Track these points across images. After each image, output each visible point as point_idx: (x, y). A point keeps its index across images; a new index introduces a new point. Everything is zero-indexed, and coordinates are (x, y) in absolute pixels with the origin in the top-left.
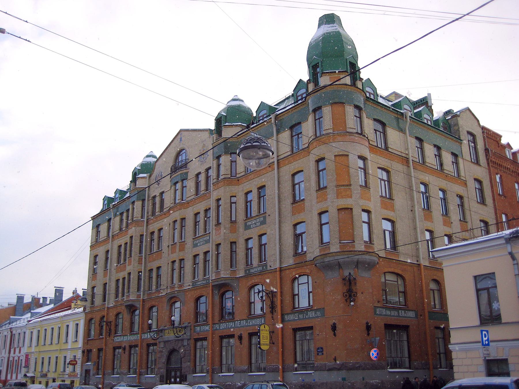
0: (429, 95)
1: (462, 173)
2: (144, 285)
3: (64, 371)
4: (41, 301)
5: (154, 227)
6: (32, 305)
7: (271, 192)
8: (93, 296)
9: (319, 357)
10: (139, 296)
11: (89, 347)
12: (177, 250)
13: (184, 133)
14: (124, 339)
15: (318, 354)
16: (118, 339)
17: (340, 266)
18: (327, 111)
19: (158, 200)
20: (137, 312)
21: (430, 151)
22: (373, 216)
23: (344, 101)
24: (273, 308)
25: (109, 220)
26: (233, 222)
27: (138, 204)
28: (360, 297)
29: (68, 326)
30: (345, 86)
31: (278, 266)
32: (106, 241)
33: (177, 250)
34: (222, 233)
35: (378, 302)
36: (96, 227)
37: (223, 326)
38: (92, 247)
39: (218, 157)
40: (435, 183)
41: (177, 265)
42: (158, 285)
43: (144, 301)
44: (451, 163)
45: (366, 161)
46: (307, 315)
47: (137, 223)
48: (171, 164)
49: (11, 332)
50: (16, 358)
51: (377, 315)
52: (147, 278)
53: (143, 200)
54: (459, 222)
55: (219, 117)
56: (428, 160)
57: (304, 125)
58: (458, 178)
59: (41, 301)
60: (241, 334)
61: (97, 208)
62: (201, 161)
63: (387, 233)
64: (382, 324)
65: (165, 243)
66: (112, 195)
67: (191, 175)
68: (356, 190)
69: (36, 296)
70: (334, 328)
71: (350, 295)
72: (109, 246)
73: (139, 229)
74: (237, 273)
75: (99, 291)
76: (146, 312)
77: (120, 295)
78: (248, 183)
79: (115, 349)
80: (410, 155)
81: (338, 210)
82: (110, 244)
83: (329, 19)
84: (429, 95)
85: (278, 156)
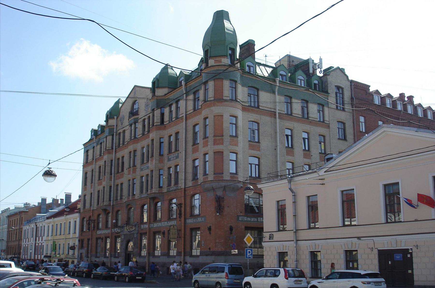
1: (327, 118)
3: (68, 254)
4: (59, 202)
7: (182, 136)
8: (85, 201)
11: (82, 238)
12: (131, 172)
13: (137, 88)
16: (99, 232)
17: (214, 189)
19: (122, 135)
20: (110, 215)
22: (239, 156)
24: (180, 214)
25: (94, 147)
26: (161, 155)
28: (226, 210)
29: (70, 222)
32: (91, 163)
33: (131, 172)
34: (154, 164)
35: (241, 212)
36: (86, 152)
37: (155, 225)
38: (84, 166)
39: (153, 110)
41: (131, 182)
42: (121, 196)
44: (316, 111)
47: (109, 151)
48: (129, 110)
49: (36, 226)
50: (40, 244)
52: (115, 190)
53: (113, 135)
54: (318, 155)
56: (294, 112)
57: (200, 91)
58: (322, 123)
59: (59, 202)
60: (164, 231)
61: (88, 137)
64: (243, 227)
65: (126, 166)
66: (96, 128)
68: (227, 139)
70: (210, 229)
71: (220, 208)
72: (93, 166)
75: (88, 198)
76: (114, 214)
77: (144, 191)
79: (97, 239)
80: (278, 108)
81: (214, 153)
85: (186, 112)
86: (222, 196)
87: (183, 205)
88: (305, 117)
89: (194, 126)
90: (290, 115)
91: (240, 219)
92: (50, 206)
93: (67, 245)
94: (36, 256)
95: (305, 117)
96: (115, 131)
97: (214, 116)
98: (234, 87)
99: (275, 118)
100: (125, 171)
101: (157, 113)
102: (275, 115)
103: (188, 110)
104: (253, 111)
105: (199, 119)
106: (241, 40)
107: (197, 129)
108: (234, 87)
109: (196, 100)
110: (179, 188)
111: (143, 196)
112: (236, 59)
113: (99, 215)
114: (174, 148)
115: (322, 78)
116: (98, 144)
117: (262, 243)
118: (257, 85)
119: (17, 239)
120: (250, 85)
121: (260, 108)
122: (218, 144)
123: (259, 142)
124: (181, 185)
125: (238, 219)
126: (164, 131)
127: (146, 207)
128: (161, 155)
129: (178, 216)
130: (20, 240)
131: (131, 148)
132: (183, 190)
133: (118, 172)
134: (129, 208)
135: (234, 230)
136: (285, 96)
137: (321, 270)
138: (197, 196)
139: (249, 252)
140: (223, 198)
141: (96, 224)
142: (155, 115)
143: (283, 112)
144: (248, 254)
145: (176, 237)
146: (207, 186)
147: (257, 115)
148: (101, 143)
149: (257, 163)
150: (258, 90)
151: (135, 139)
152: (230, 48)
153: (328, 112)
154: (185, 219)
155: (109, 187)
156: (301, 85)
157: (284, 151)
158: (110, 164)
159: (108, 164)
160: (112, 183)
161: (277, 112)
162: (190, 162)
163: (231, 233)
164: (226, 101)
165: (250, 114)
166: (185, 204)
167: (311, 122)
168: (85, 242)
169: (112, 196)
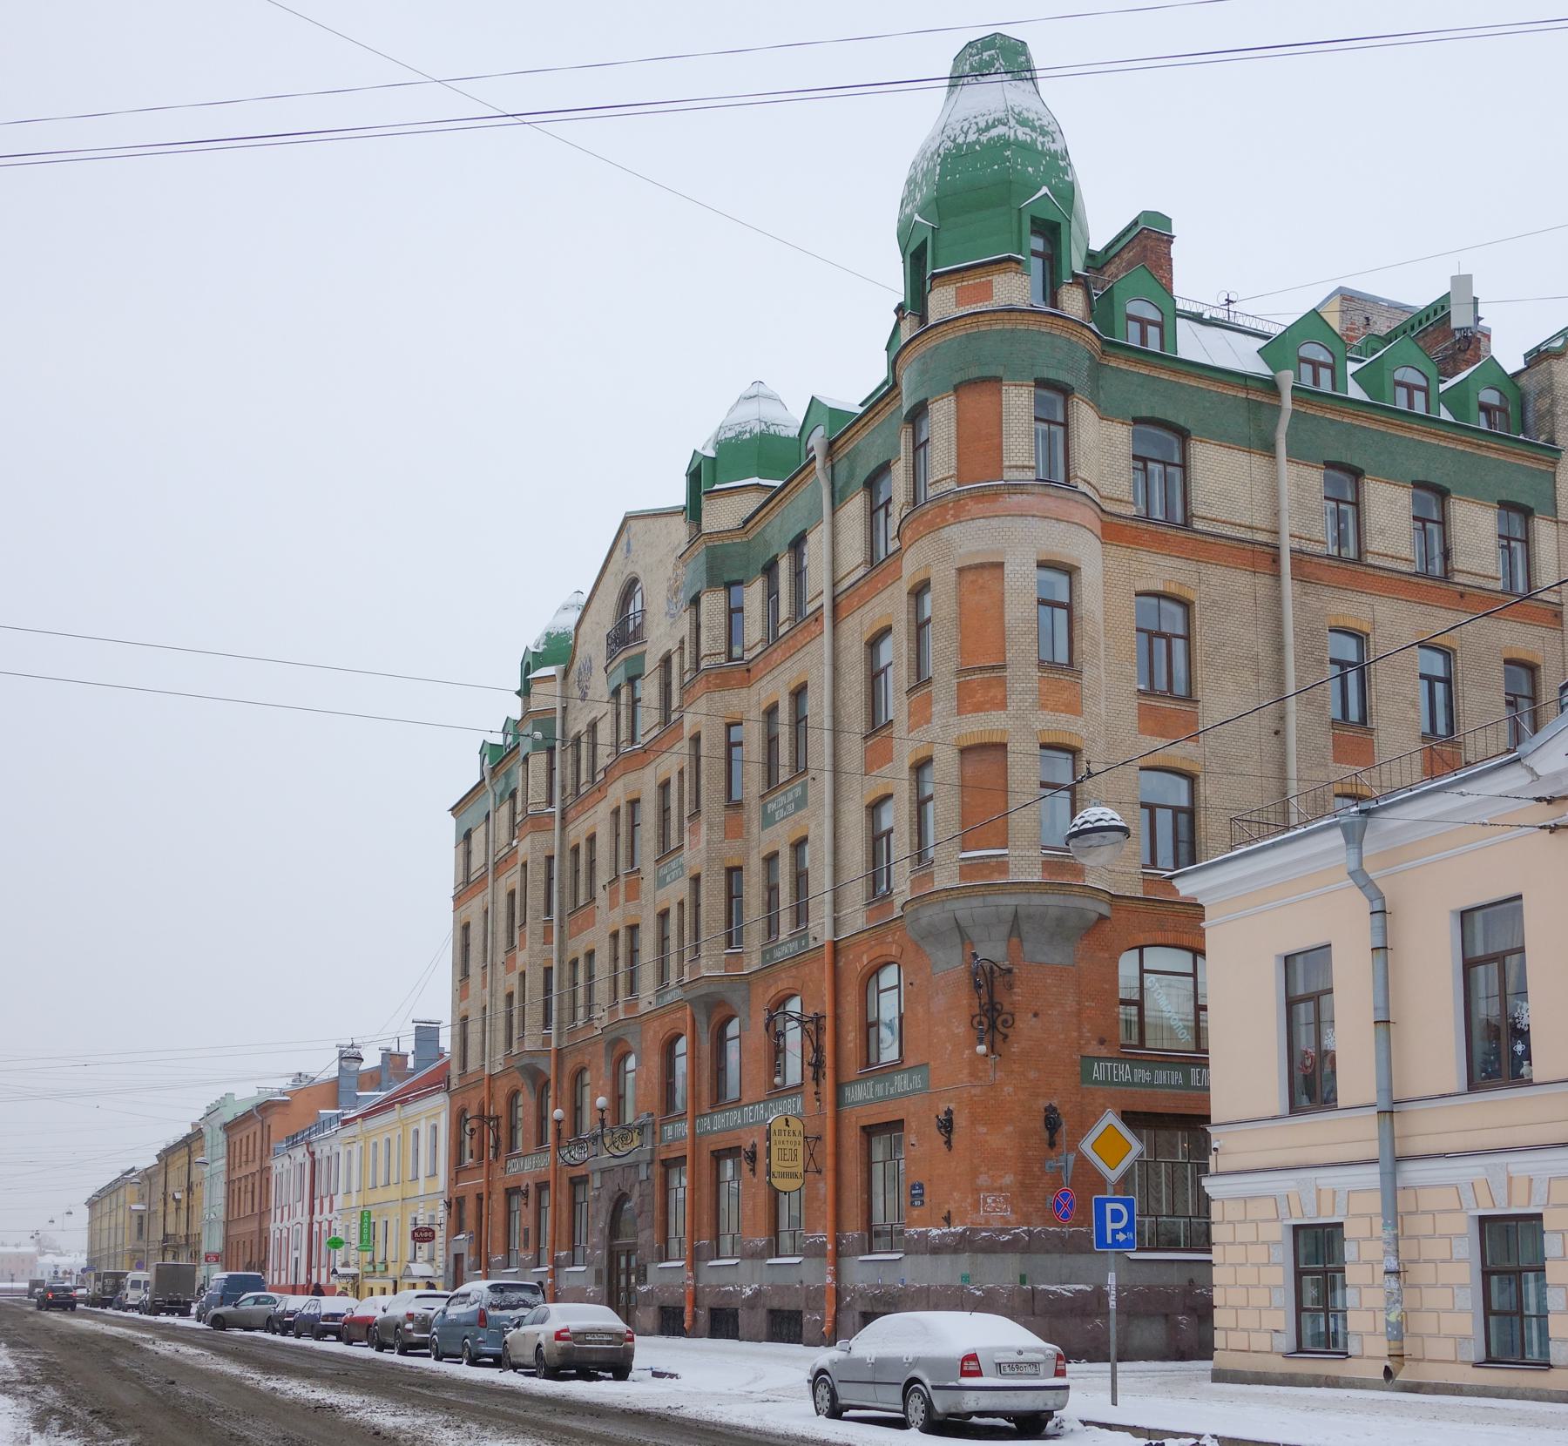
0: (1462, 282)
1: (1547, 575)
2: (560, 1009)
5: (577, 833)
6: (385, 1076)
7: (818, 706)
9: (915, 1213)
10: (547, 1040)
13: (635, 525)
14: (527, 1167)
15: (912, 1204)
16: (514, 1167)
18: (942, 414)
21: (1389, 510)
23: (999, 372)
24: (818, 1066)
26: (734, 805)
27: (539, 761)
28: (1025, 1025)
30: (1006, 316)
31: (827, 936)
34: (703, 844)
35: (1102, 1042)
37: (720, 1121)
38: (459, 899)
39: (695, 601)
40: (1395, 622)
43: (559, 1051)
45: (1074, 576)
46: (892, 1085)
47: (538, 823)
50: (325, 1226)
51: (1096, 1082)
53: (551, 750)
55: (695, 465)
62: (673, 616)
63: (1164, 819)
67: (651, 663)
68: (1023, 678)
69: (394, 1049)
70: (947, 1126)
71: (992, 1019)
73: (541, 838)
74: (746, 961)
76: (566, 1084)
78: (769, 677)
79: (510, 1193)
80: (1287, 527)
82: (826, 637)
83: (998, 57)
84: (1462, 282)
85: (834, 585)
86: (1006, 965)
87: (828, 1023)
88: (1435, 578)
89: (874, 644)
90: (1349, 564)
91: (1098, 1072)
92: (374, 1079)
93: (410, 1221)
94: (315, 1271)
95: (1435, 578)
96: (558, 735)
97: (960, 570)
98: (1060, 419)
99: (1277, 575)
100: (602, 896)
101: (714, 604)
102: (1276, 560)
103: (842, 573)
104: (1159, 544)
105: (891, 605)
106: (1101, 223)
107: (886, 652)
108: (1060, 419)
109: (876, 509)
110: (812, 945)
111: (669, 998)
112: (1065, 272)
113: (513, 1096)
114: (785, 762)
115: (1523, 381)
116: (502, 801)
117: (1205, 1182)
118: (1179, 412)
119: (256, 1210)
120: (1145, 413)
121: (1198, 525)
122: (978, 708)
123: (1190, 698)
124: (821, 928)
125: (1086, 1075)
126: (744, 691)
127: (682, 1046)
128: (734, 805)
129: (809, 1072)
130: (264, 1214)
131: (617, 793)
132: (827, 951)
133: (576, 908)
134: (616, 1053)
135: (1064, 1128)
136: (1330, 465)
137: (1542, 1316)
138: (889, 977)
139: (1117, 1216)
140: (1009, 971)
141: (503, 1133)
142: (704, 619)
143: (1318, 549)
144: (1110, 1226)
145: (800, 1169)
146: (929, 915)
147: (1178, 563)
148: (513, 795)
149: (1184, 802)
150: (1183, 435)
151: (633, 757)
152: (1034, 220)
153: (1554, 545)
154: (839, 1088)
155: (541, 973)
156: (1411, 405)
157: (1325, 740)
158: (542, 877)
159: (537, 875)
160: (555, 956)
161: (1287, 545)
162: (854, 817)
163: (1052, 1145)
164: (1017, 488)
165: (1144, 556)
166: (837, 1018)
167: (1462, 595)
168: (470, 1206)
169: (554, 1014)
